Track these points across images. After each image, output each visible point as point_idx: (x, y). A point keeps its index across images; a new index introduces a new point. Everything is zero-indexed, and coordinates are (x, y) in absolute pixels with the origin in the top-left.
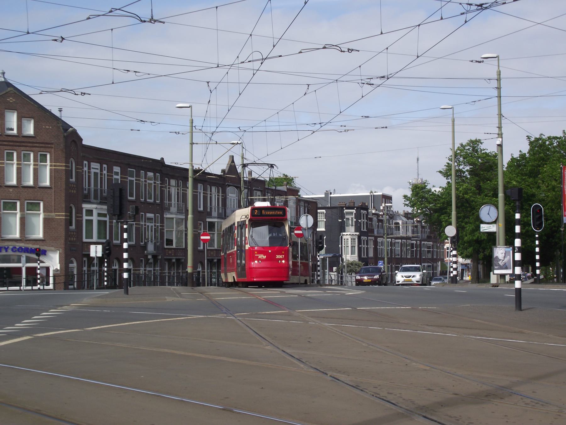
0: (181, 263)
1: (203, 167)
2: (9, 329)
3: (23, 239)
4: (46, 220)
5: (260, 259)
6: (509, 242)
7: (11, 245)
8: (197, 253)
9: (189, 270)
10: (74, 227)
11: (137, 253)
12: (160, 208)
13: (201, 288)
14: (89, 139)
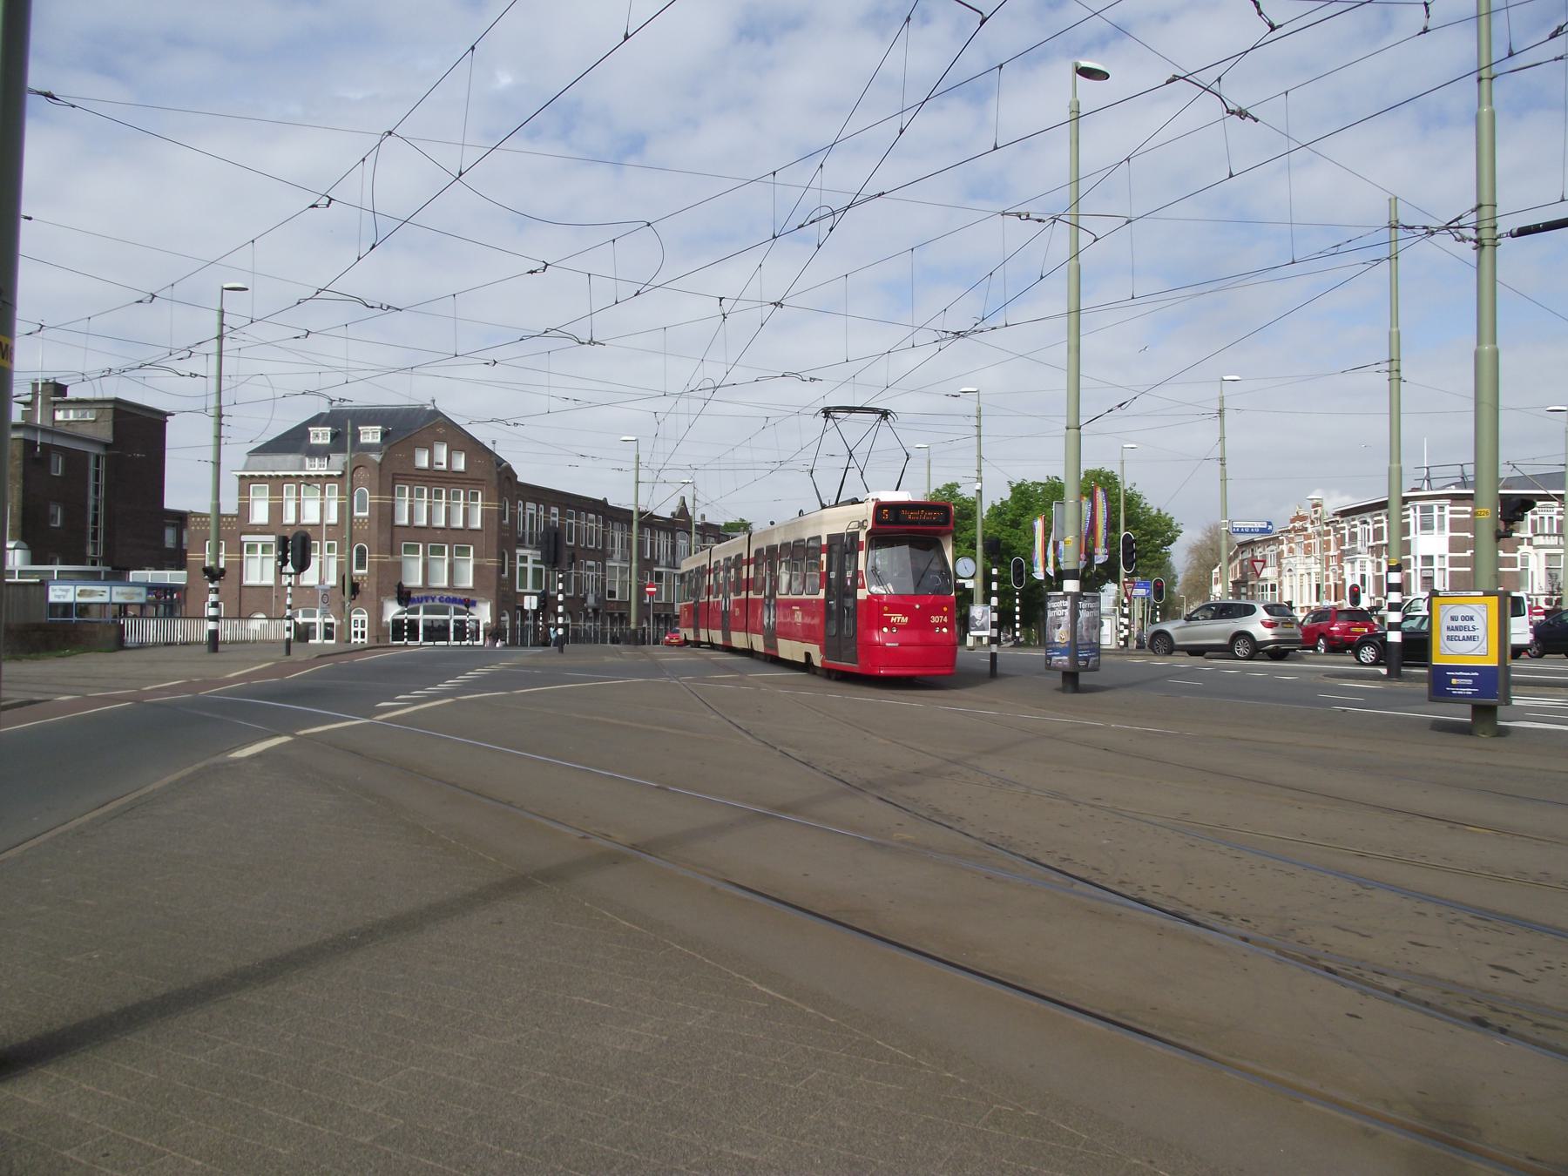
0: (624, 618)
1: (650, 509)
2: (431, 690)
3: (451, 588)
4: (475, 567)
5: (894, 625)
6: (987, 601)
7: (438, 595)
8: (642, 607)
9: (633, 626)
10: (506, 575)
11: (575, 606)
12: (603, 555)
13: (646, 647)
14: (527, 474)
